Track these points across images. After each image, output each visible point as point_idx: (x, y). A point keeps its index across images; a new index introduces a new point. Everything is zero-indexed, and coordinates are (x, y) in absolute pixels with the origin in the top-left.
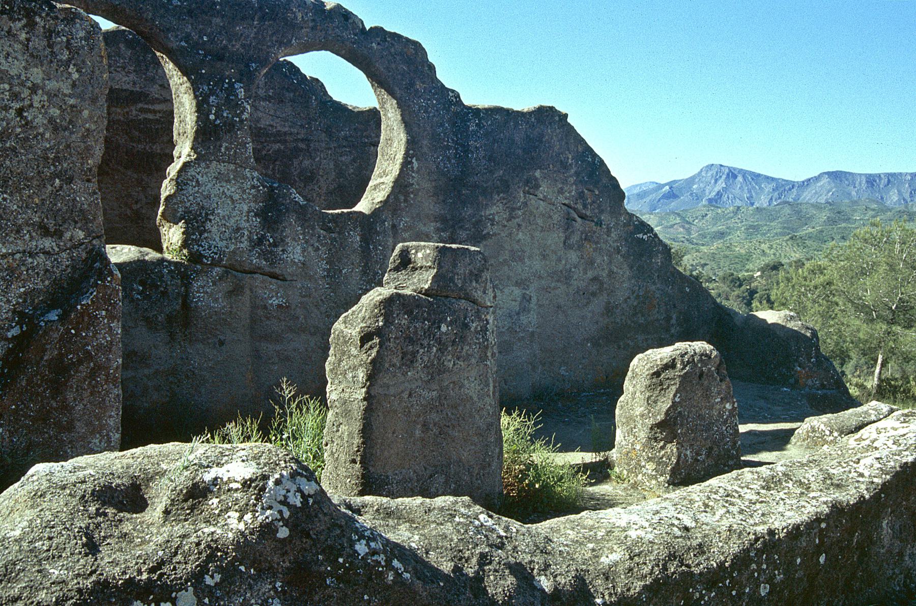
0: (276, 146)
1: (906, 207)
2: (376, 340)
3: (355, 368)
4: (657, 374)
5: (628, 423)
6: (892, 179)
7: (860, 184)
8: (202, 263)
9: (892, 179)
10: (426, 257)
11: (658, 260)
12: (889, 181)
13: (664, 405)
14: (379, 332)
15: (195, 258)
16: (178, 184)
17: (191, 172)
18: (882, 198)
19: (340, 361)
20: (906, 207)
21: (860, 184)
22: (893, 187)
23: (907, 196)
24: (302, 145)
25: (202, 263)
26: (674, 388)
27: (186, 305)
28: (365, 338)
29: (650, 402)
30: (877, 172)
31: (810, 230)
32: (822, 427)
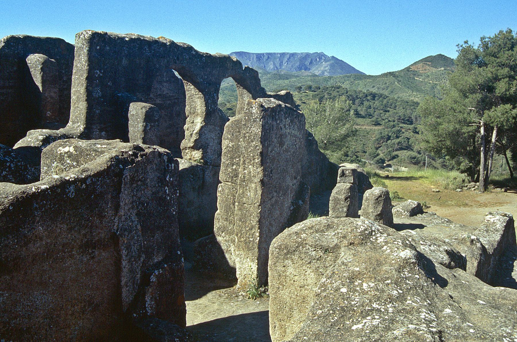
0: (168, 102)
1: (278, 72)
2: (349, 199)
3: (343, 207)
4: (377, 199)
5: (366, 215)
6: (270, 56)
7: (253, 59)
8: (208, 165)
9: (270, 56)
10: (349, 173)
11: (314, 147)
12: (268, 57)
13: (380, 209)
14: (349, 197)
15: (206, 163)
16: (200, 135)
17: (203, 130)
18: (265, 67)
19: (336, 205)
20: (278, 72)
21: (253, 59)
22: (270, 61)
23: (278, 65)
24: (176, 101)
25: (208, 165)
26: (382, 203)
27: (203, 182)
28: (346, 199)
29: (375, 208)
30: (262, 52)
31: (226, 85)
32: (401, 210)
